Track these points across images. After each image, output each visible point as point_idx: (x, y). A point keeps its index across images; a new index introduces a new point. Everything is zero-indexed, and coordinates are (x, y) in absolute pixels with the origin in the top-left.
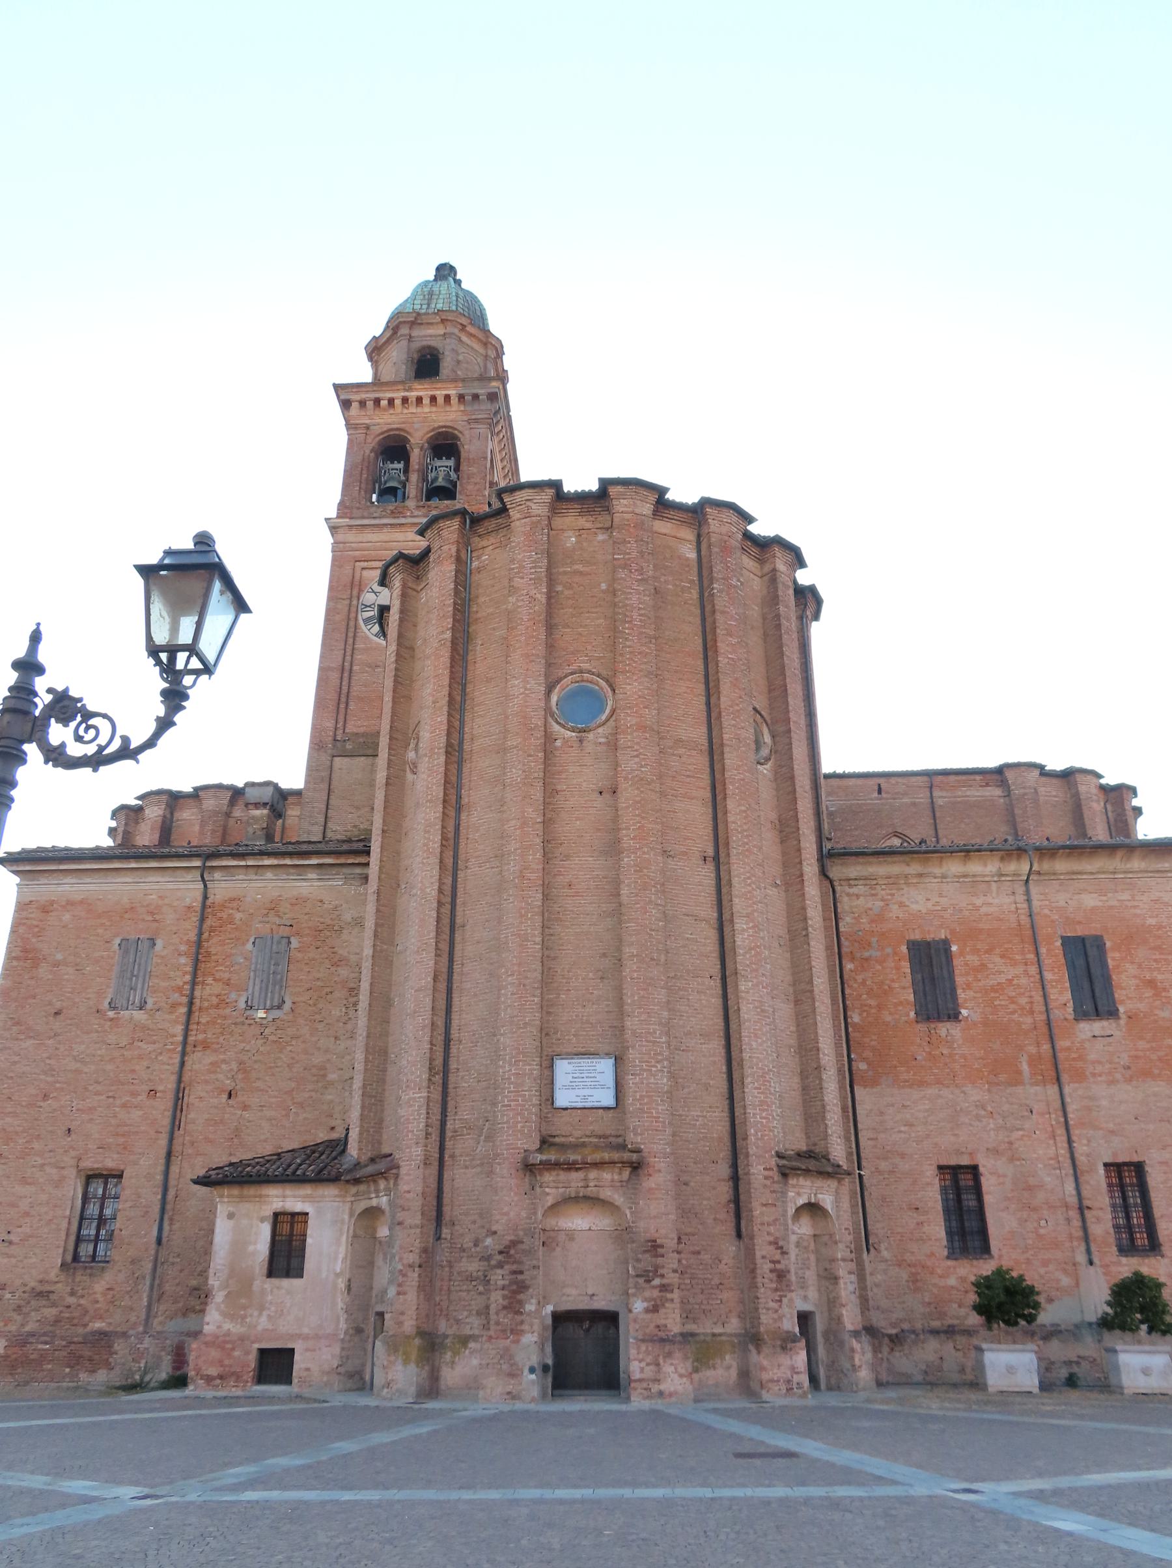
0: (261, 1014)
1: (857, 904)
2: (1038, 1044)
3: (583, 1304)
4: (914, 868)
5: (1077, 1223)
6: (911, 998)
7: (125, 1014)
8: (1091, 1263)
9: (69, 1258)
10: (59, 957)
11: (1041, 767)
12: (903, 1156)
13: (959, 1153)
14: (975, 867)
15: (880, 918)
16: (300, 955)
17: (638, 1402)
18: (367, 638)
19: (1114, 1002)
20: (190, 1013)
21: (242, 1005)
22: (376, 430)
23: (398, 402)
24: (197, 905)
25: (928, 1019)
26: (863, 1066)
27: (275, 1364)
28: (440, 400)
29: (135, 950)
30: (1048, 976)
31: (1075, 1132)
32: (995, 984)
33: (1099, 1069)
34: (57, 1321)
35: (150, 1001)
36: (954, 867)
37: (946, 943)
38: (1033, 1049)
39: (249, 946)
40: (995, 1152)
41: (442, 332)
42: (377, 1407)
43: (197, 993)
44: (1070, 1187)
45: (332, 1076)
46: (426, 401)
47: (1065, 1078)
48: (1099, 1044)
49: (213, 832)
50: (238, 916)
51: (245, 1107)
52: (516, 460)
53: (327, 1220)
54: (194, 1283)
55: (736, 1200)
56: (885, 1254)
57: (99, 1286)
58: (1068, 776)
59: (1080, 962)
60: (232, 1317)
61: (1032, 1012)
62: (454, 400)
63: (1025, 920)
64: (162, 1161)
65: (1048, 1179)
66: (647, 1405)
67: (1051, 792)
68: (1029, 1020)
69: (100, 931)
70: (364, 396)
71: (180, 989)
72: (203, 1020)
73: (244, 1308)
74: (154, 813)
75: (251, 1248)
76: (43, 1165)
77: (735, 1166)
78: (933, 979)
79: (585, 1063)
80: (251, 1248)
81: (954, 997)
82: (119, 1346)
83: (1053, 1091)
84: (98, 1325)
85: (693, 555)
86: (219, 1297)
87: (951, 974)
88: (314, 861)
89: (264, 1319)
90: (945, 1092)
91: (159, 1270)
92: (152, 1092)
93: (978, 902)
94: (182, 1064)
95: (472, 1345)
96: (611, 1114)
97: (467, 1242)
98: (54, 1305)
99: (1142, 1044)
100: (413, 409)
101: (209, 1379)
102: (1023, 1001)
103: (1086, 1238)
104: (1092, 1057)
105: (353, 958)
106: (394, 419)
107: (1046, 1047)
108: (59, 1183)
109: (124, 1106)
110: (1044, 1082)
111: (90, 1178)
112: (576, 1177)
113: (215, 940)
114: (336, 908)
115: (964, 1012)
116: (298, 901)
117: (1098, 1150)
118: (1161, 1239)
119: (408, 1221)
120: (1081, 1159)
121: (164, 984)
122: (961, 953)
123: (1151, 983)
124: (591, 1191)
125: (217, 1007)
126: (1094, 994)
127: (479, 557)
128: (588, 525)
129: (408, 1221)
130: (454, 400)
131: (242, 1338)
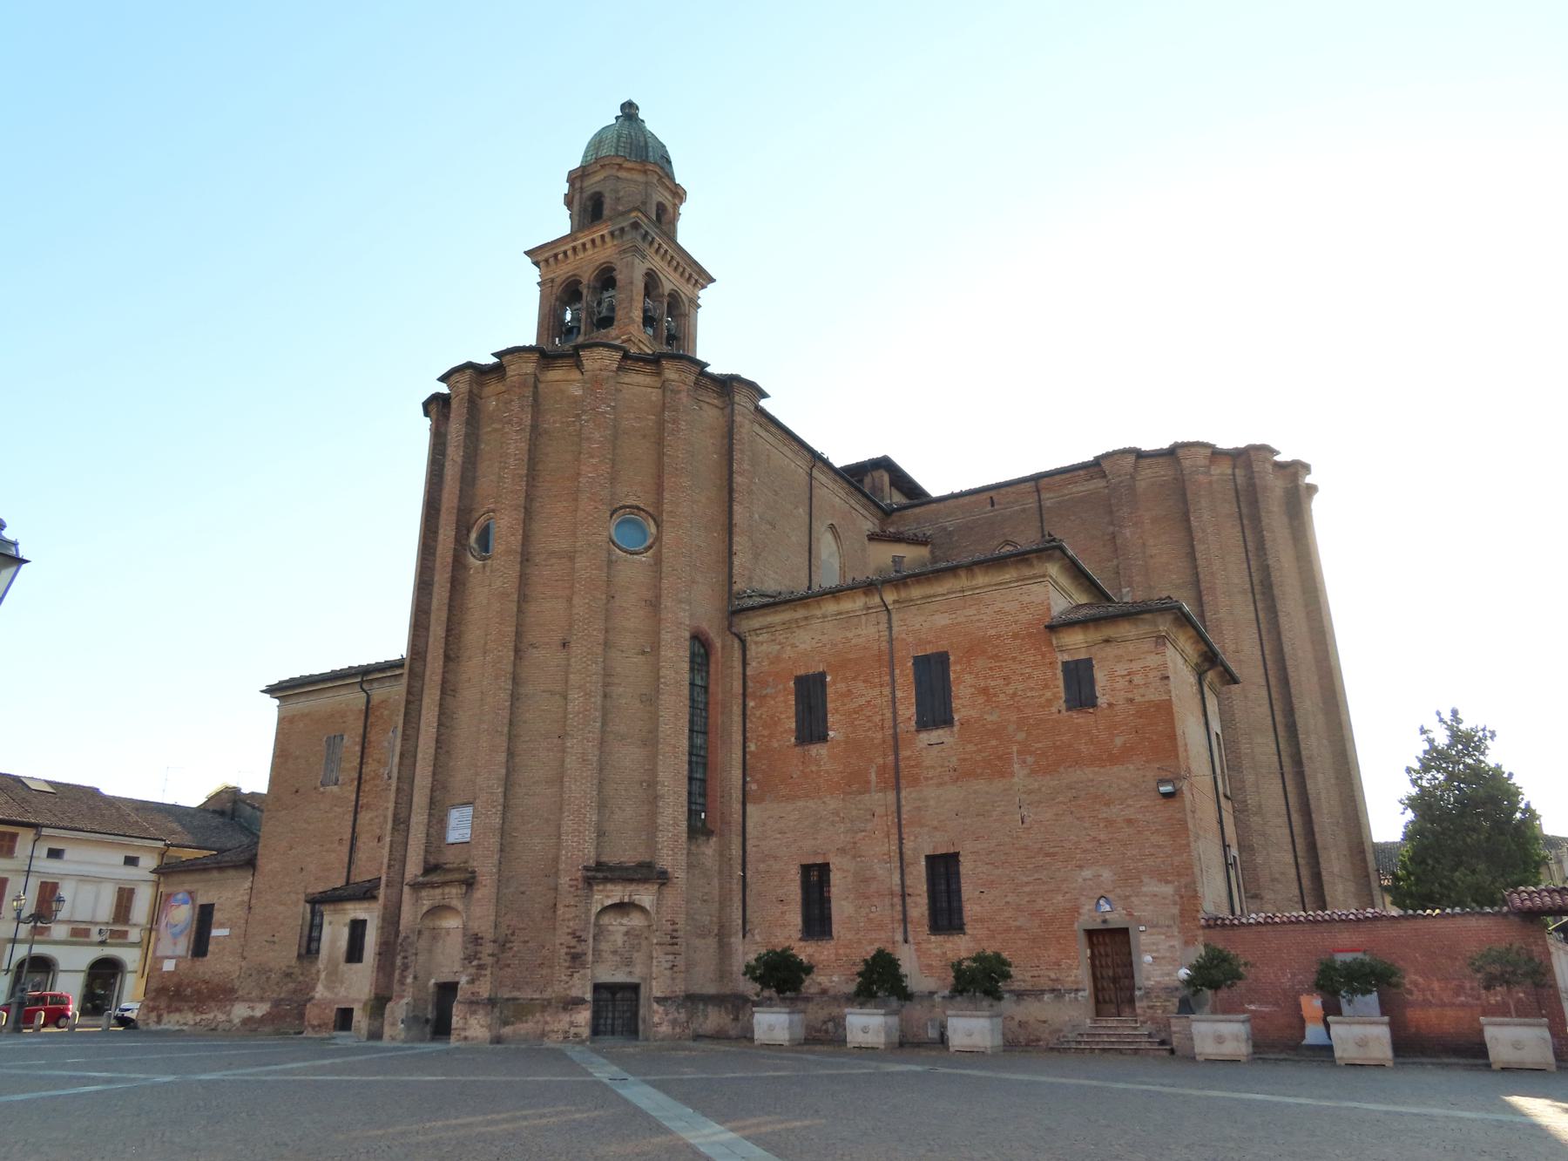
1: (761, 648)
2: (885, 755)
4: (800, 613)
5: (899, 908)
6: (793, 726)
8: (906, 941)
9: (303, 951)
12: (775, 858)
13: (816, 853)
15: (777, 659)
17: (454, 1042)
19: (951, 711)
22: (559, 281)
26: (754, 787)
28: (598, 242)
30: (899, 694)
31: (905, 830)
32: (866, 706)
36: (830, 607)
37: (823, 675)
40: (842, 851)
44: (896, 879)
46: (589, 246)
47: (903, 782)
52: (696, 263)
56: (758, 938)
61: (882, 728)
62: (608, 239)
63: (884, 646)
65: (880, 870)
68: (879, 735)
83: (891, 796)
90: (811, 804)
93: (850, 635)
99: (970, 748)
100: (581, 255)
101: (313, 1027)
102: (877, 719)
103: (905, 920)
104: (927, 763)
115: (831, 734)
117: (922, 844)
118: (966, 920)
120: (908, 853)
122: (834, 682)
126: (935, 709)
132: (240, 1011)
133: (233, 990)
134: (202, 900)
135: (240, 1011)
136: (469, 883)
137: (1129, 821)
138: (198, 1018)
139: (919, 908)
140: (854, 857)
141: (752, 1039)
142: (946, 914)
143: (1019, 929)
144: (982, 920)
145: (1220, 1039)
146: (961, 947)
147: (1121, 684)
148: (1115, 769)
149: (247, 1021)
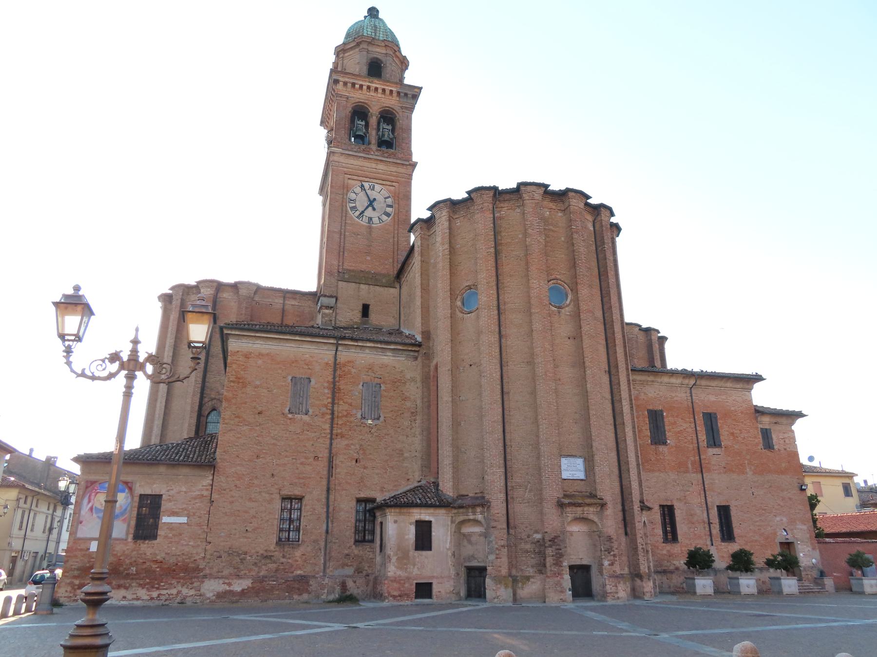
0: (370, 422)
3: (578, 563)
4: (651, 378)
5: (707, 529)
7: (299, 416)
10: (258, 383)
11: (640, 326)
13: (667, 500)
14: (673, 380)
16: (386, 394)
17: (610, 601)
18: (352, 218)
20: (332, 419)
21: (359, 416)
22: (352, 101)
23: (365, 88)
24: (331, 362)
25: (656, 444)
27: (424, 590)
28: (388, 92)
29: (300, 385)
30: (698, 428)
33: (715, 468)
34: (277, 570)
35: (311, 411)
37: (662, 411)
38: (692, 459)
39: (360, 387)
40: (679, 500)
41: (384, 52)
42: (556, 607)
43: (336, 408)
44: (705, 515)
45: (406, 455)
46: (380, 91)
47: (704, 470)
48: (715, 458)
49: (246, 308)
50: (353, 371)
51: (365, 468)
53: (442, 525)
54: (346, 552)
55: (624, 519)
57: (298, 553)
58: (648, 331)
59: (709, 423)
60: (401, 569)
62: (395, 94)
64: (325, 492)
66: (614, 602)
67: (641, 337)
68: (691, 446)
69: (280, 371)
70: (347, 80)
71: (326, 406)
72: (340, 423)
73: (406, 564)
74: (207, 292)
75: (407, 537)
76: (260, 492)
77: (623, 505)
78: (657, 426)
79: (572, 460)
80: (407, 537)
81: (665, 435)
82: (312, 582)
83: (700, 476)
84: (299, 572)
85: (592, 229)
86: (394, 559)
87: (664, 426)
88: (392, 347)
89: (416, 569)
90: (662, 475)
91: (328, 546)
92: (316, 458)
94: (331, 444)
95: (532, 580)
96: (583, 482)
97: (524, 536)
98: (275, 562)
99: (729, 458)
101: (394, 597)
102: (689, 438)
104: (713, 463)
105: (412, 397)
106: (362, 96)
107: (697, 458)
108: (270, 501)
109: (302, 464)
110: (696, 472)
111: (284, 499)
112: (579, 510)
113: (342, 382)
114: (402, 372)
116: (384, 366)
117: (716, 500)
119: (499, 527)
120: (709, 504)
121: (318, 402)
122: (667, 416)
123: (732, 434)
124: (585, 515)
125: (346, 416)
126: (714, 441)
127: (500, 212)
128: (554, 207)
129: (499, 527)
130: (395, 94)
131: (408, 578)
132: (211, 587)
133: (197, 569)
134: (142, 488)
135: (211, 587)
136: (603, 506)
137: (790, 499)
138: (155, 594)
139: (716, 530)
140: (686, 503)
141: (695, 593)
142: (727, 534)
143: (756, 541)
144: (742, 536)
145: (871, 586)
146: (734, 547)
147: (782, 442)
148: (783, 477)
149: (220, 596)
